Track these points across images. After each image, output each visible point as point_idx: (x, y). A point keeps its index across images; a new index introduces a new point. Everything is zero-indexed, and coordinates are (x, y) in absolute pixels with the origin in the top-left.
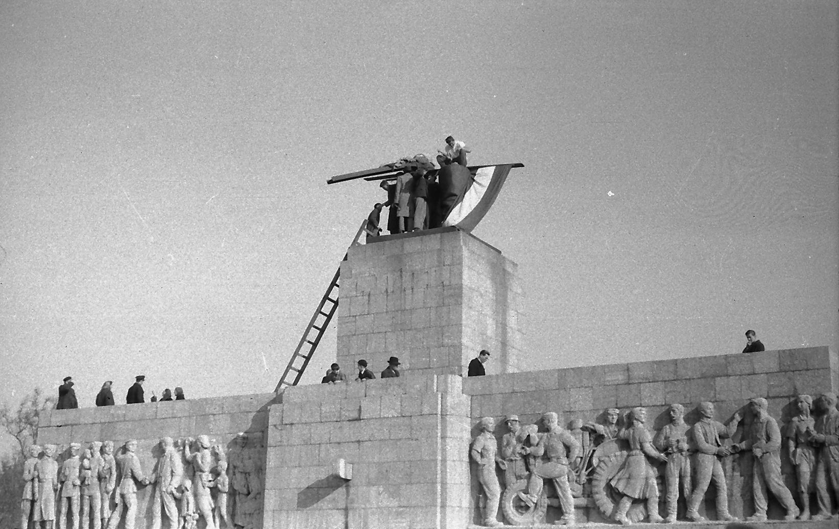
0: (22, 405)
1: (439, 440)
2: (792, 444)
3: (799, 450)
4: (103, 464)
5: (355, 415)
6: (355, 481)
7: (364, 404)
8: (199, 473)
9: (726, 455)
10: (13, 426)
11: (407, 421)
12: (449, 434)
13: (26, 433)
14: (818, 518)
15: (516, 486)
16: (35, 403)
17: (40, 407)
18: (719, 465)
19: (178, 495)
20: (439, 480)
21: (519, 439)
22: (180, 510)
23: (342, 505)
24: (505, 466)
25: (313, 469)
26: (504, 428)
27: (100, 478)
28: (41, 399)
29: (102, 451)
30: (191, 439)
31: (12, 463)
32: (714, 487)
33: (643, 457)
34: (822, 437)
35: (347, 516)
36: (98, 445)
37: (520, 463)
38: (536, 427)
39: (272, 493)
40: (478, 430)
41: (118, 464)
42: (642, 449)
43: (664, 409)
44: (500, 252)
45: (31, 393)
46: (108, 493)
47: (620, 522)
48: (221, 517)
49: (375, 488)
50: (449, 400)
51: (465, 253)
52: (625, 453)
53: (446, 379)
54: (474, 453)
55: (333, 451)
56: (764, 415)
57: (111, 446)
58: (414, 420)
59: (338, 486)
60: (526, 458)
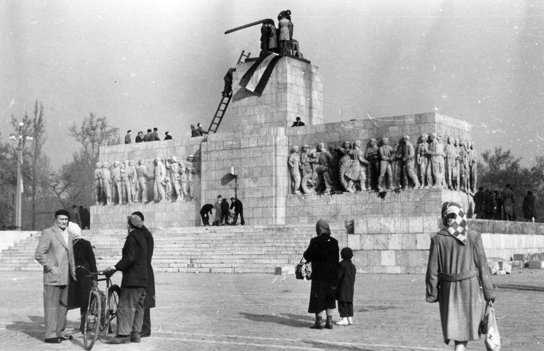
0: (84, 123)
1: (274, 157)
2: (419, 155)
3: (421, 158)
4: (130, 170)
5: (238, 146)
6: (239, 176)
7: (242, 141)
8: (172, 174)
9: (392, 161)
10: (80, 137)
11: (260, 149)
12: (278, 154)
13: (87, 140)
14: (427, 187)
15: (307, 176)
16: (91, 122)
17: (94, 125)
18: (389, 166)
19: (164, 184)
20: (274, 175)
21: (308, 156)
22: (166, 190)
23: (234, 186)
24: (303, 167)
25: (221, 171)
26: (303, 150)
27: (129, 177)
28: (95, 120)
29: (129, 164)
30: (169, 158)
31: (79, 158)
32: (387, 174)
33: (358, 163)
34: (430, 152)
35: (236, 192)
36: (127, 161)
37: (309, 166)
38: (315, 150)
39: (204, 182)
40: (292, 151)
41: (137, 170)
42: (358, 159)
43: (368, 141)
44: (309, 62)
45: (88, 116)
46: (133, 184)
47: (349, 191)
48: (184, 193)
49: (247, 179)
50: (278, 139)
51: (288, 67)
52: (352, 160)
53: (277, 129)
54: (290, 162)
55: (230, 163)
56: (408, 143)
57: (133, 162)
58: (263, 148)
59: (232, 178)
60: (311, 164)
